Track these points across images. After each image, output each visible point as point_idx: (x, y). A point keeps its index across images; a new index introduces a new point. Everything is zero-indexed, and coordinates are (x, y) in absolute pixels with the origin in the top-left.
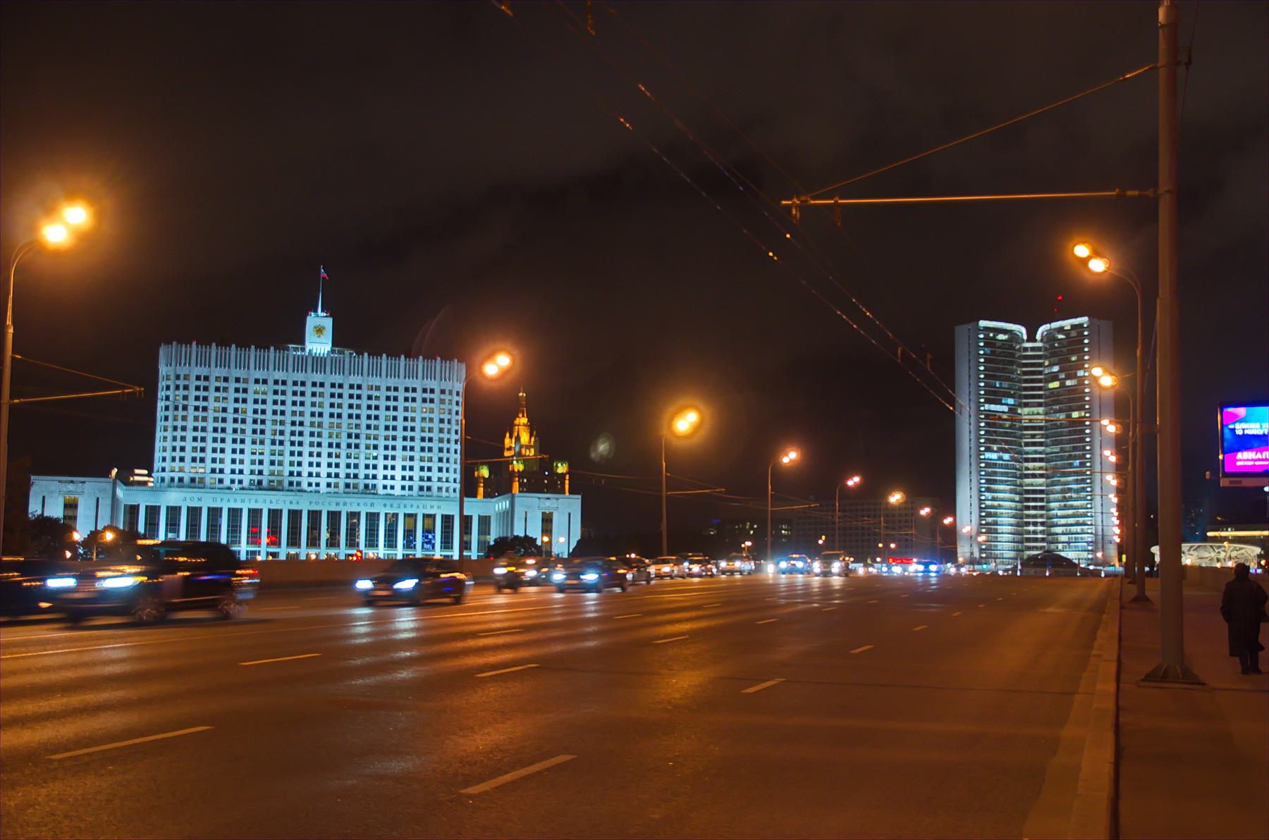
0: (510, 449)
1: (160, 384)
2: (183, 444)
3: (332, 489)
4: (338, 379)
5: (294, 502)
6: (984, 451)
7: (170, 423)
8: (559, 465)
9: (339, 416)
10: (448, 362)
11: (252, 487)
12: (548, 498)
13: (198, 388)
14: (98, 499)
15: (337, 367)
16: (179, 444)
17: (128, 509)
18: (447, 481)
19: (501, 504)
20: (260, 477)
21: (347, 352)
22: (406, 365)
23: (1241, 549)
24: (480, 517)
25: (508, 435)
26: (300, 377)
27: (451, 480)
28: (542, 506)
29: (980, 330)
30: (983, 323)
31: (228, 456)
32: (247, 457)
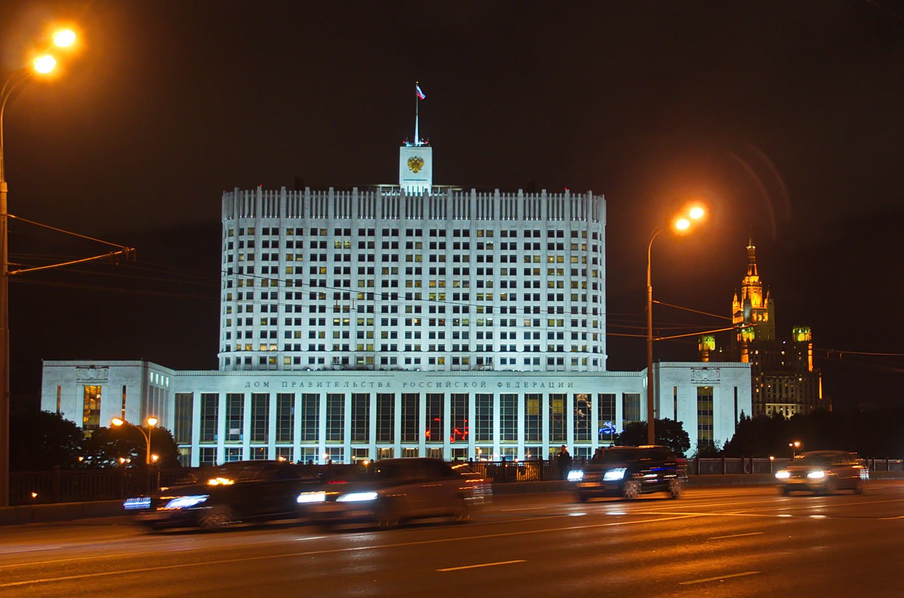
9: (443, 271)
12: (705, 368)
14: (124, 387)
15: (437, 208)
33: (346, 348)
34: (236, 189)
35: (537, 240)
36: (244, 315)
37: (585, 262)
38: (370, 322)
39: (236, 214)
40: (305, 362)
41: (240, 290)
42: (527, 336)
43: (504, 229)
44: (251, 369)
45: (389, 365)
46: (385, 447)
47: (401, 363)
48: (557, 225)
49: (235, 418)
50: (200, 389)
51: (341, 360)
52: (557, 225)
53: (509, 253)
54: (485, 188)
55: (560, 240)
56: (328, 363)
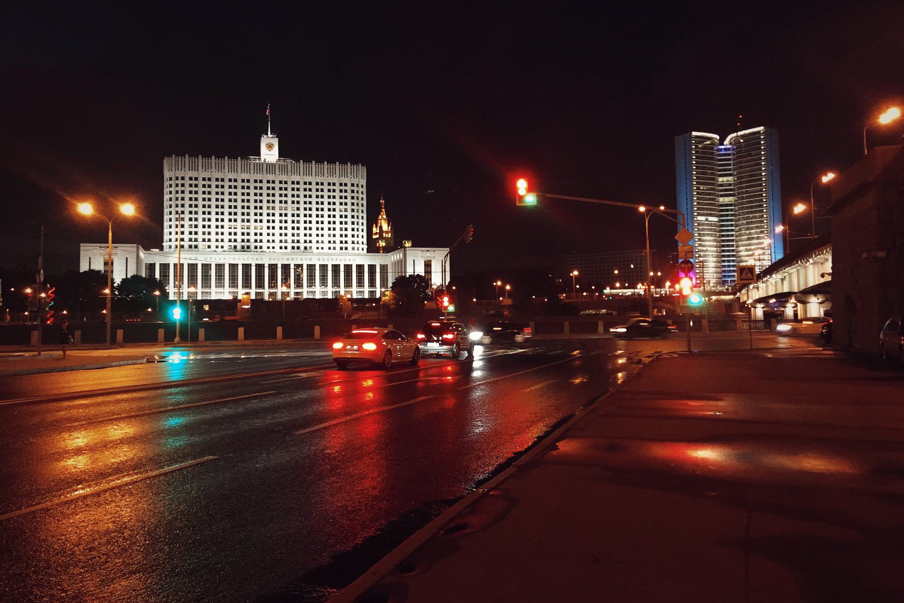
0: (376, 234)
1: (165, 184)
2: (183, 202)
4: (284, 178)
5: (222, 259)
6: (697, 215)
8: (406, 242)
9: (286, 202)
10: (355, 165)
11: (230, 250)
12: (428, 251)
13: (191, 192)
14: (127, 258)
15: (283, 169)
16: (180, 196)
17: (148, 267)
19: (396, 256)
20: (235, 244)
21: (289, 161)
22: (328, 168)
25: (374, 226)
26: (259, 177)
27: (360, 242)
28: (424, 256)
29: (693, 138)
30: (694, 133)
31: (213, 230)
33: (235, 241)
34: (173, 156)
35: (310, 187)
38: (235, 227)
40: (213, 248)
43: (305, 181)
44: (236, 251)
45: (258, 250)
46: (192, 289)
47: (265, 248)
48: (344, 180)
50: (159, 261)
51: (233, 246)
52: (344, 180)
53: (320, 193)
54: (307, 160)
55: (346, 188)
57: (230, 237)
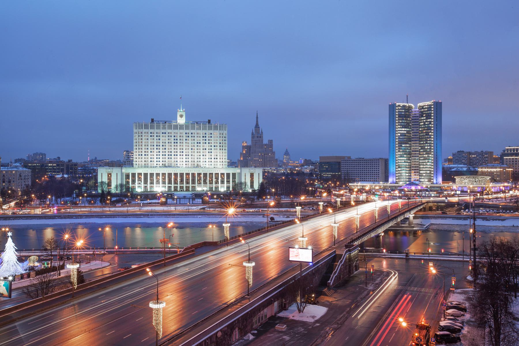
3: (187, 166)
5: (159, 171)
7: (137, 147)
18: (222, 162)
20: (165, 163)
23: (484, 177)
24: (233, 174)
27: (224, 161)
32: (196, 157)
33: (165, 161)
36: (140, 153)
37: (223, 141)
39: (138, 128)
41: (139, 147)
42: (209, 158)
49: (140, 179)
56: (161, 165)
57: (157, 160)
